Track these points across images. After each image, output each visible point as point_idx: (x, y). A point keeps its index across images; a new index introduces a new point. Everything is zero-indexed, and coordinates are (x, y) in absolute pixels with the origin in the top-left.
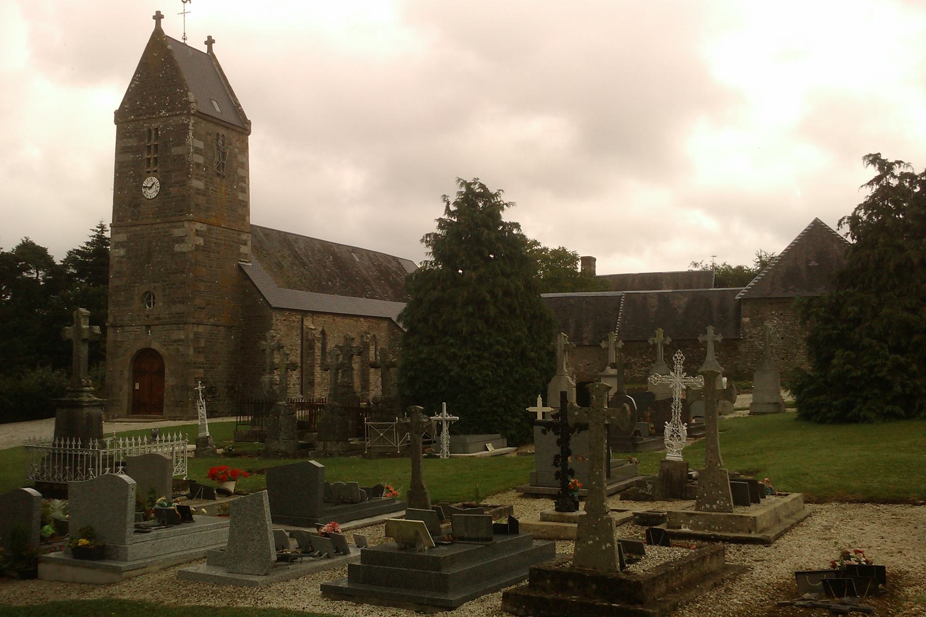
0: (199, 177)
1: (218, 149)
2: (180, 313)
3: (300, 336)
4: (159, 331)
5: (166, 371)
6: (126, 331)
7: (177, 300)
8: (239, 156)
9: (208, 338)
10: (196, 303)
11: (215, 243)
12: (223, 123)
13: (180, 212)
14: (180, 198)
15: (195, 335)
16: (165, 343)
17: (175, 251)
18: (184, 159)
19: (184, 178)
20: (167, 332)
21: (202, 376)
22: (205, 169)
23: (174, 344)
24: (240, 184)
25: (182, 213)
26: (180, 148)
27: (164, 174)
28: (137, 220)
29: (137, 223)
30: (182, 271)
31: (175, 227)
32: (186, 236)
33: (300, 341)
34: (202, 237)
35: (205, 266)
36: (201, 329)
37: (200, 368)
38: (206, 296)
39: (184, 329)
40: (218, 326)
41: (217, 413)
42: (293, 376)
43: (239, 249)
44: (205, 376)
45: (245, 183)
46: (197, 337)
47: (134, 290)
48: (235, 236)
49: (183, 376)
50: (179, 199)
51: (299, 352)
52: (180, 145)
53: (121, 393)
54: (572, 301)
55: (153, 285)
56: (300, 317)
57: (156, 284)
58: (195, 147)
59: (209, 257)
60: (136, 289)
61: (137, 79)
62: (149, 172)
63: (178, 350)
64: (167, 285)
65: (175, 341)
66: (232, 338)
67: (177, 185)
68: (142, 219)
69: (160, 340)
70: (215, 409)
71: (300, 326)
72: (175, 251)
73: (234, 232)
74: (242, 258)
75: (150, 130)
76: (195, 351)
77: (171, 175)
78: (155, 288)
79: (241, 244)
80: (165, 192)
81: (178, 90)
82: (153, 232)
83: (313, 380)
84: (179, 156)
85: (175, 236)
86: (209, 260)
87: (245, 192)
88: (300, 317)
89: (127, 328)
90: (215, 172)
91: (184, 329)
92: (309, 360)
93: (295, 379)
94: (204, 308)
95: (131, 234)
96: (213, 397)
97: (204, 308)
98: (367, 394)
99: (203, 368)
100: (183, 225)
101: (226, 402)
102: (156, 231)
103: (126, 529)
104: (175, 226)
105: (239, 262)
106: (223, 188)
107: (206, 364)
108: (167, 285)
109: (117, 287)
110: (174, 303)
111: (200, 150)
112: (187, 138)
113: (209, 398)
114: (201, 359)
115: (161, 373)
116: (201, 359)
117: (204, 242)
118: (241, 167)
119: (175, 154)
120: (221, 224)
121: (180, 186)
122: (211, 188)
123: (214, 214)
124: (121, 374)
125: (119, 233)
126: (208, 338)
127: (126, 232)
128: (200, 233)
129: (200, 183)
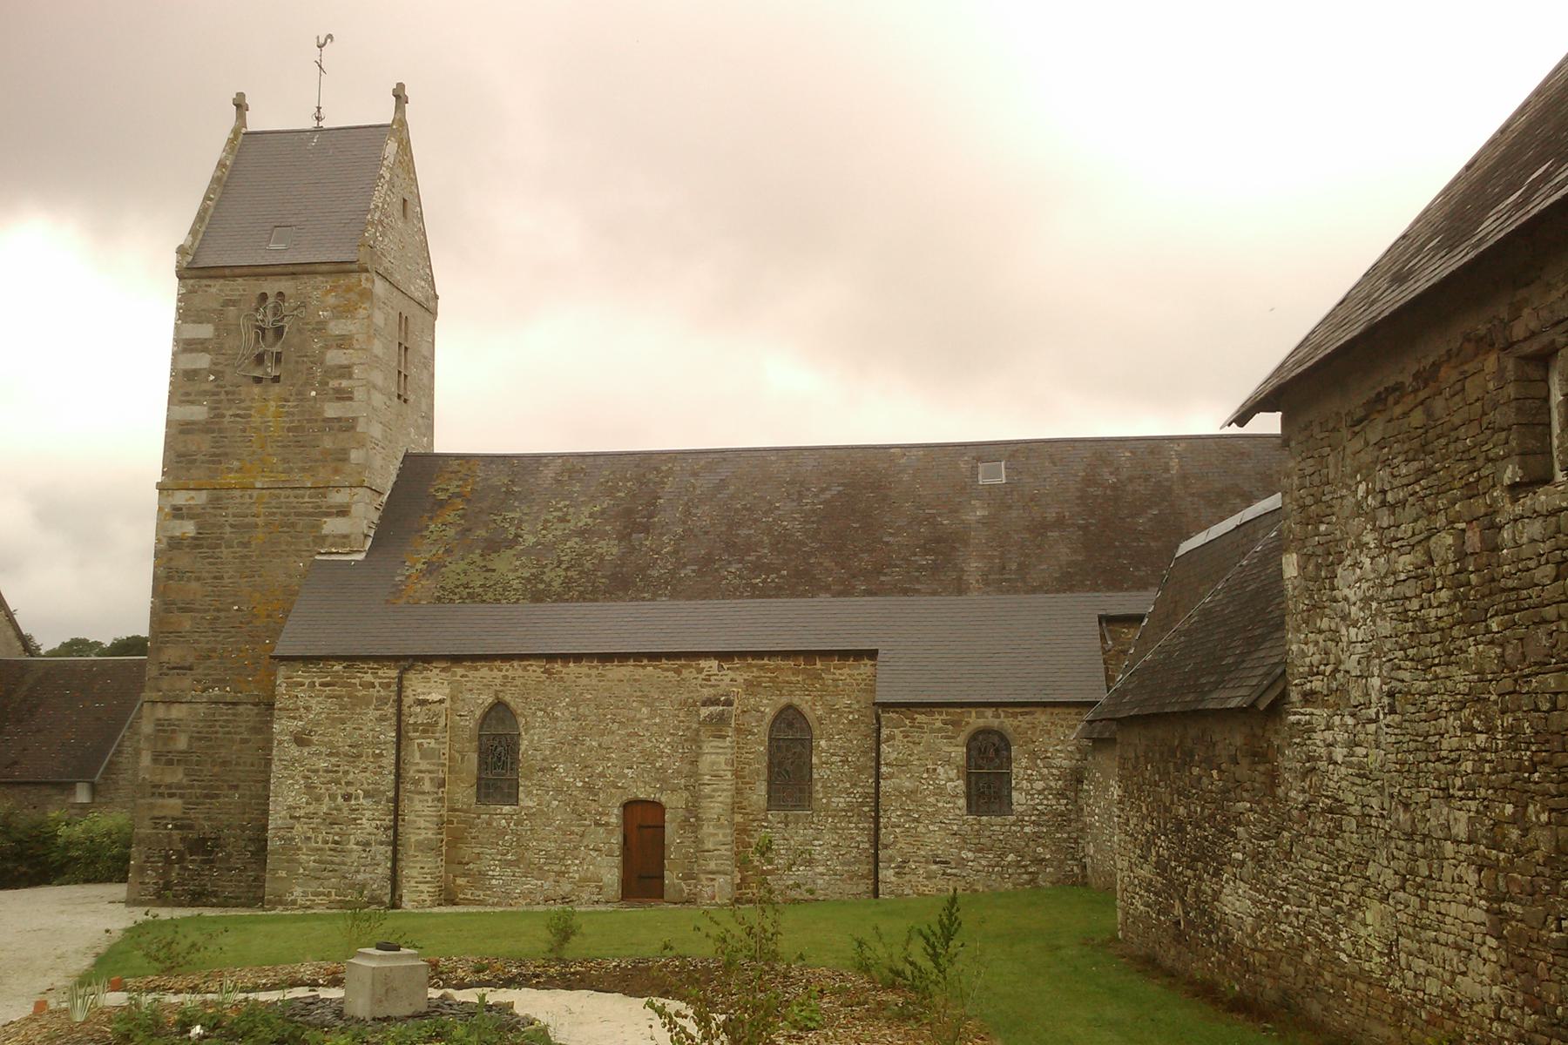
9: (199, 732)
10: (164, 658)
12: (271, 270)
15: (157, 725)
21: (178, 814)
34: (191, 518)
35: (198, 579)
36: (177, 712)
38: (196, 642)
40: (235, 704)
41: (216, 896)
42: (364, 821)
44: (184, 813)
56: (394, 673)
70: (209, 888)
71: (394, 696)
73: (302, 492)
74: (332, 545)
76: (155, 760)
88: (394, 673)
94: (190, 668)
96: (205, 862)
97: (190, 668)
99: (182, 796)
103: (1499, 917)
106: (272, 403)
107: (192, 787)
113: (192, 861)
114: (177, 776)
116: (177, 776)
120: (253, 483)
123: (236, 464)
126: (199, 732)
128: (184, 511)
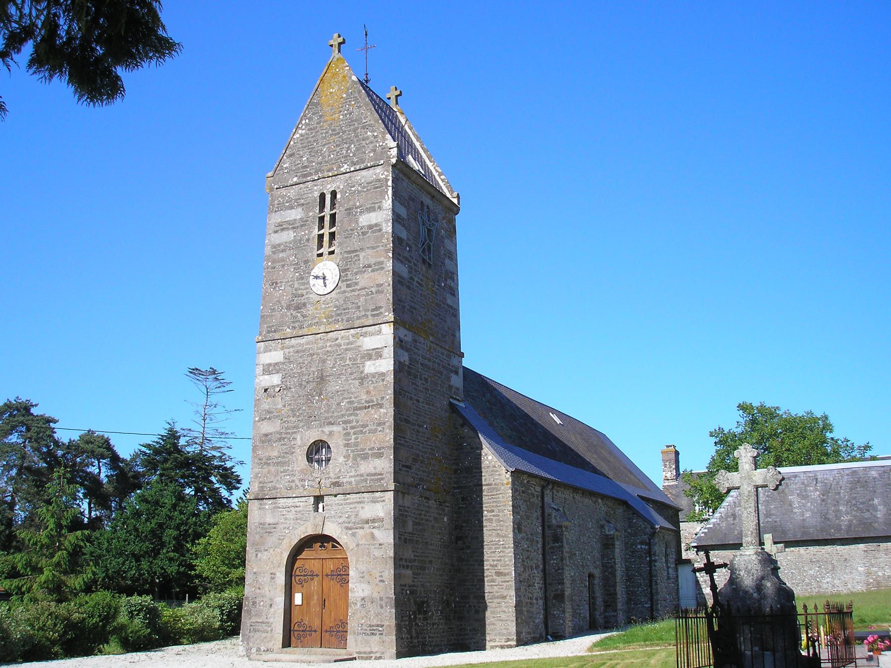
0: (401, 258)
1: (423, 224)
2: (375, 474)
3: (540, 520)
4: (339, 505)
5: (352, 573)
6: (280, 505)
7: (370, 452)
8: (446, 241)
11: (422, 364)
13: (373, 310)
14: (374, 290)
16: (349, 525)
17: (366, 372)
18: (380, 230)
19: (382, 259)
20: (352, 506)
22: (408, 249)
23: (366, 526)
24: (449, 281)
25: (378, 312)
26: (373, 215)
27: (346, 256)
28: (301, 328)
29: (300, 333)
30: (378, 404)
31: (364, 335)
32: (386, 347)
33: (540, 528)
35: (411, 399)
37: (407, 567)
39: (384, 501)
43: (449, 378)
45: (454, 281)
46: (402, 515)
47: (296, 439)
48: (445, 357)
49: (382, 581)
50: (372, 291)
51: (540, 545)
52: (374, 210)
53: (272, 610)
54: (873, 472)
55: (327, 429)
57: (335, 428)
58: (397, 213)
59: (415, 384)
60: (299, 437)
61: (304, 127)
62: (320, 255)
63: (373, 536)
64: (352, 428)
65: (367, 522)
66: (445, 520)
67: (370, 269)
68: (311, 325)
69: (340, 521)
72: (366, 372)
75: (322, 196)
77: (358, 256)
78: (331, 433)
79: (452, 371)
80: (348, 283)
81: (369, 133)
82: (328, 345)
83: (563, 591)
84: (370, 227)
85: (365, 348)
86: (416, 389)
87: (454, 295)
89: (281, 501)
90: (420, 255)
91: (384, 501)
92: (554, 559)
93: (538, 590)
95: (291, 350)
98: (614, 616)
100: (380, 331)
101: (441, 627)
102: (333, 343)
104: (366, 333)
105: (451, 400)
108: (352, 428)
109: (266, 435)
110: (365, 457)
111: (403, 220)
112: (384, 199)
115: (341, 576)
117: (410, 359)
118: (449, 257)
119: (365, 224)
121: (373, 271)
122: (416, 279)
124: (273, 578)
125: (270, 351)
127: (282, 348)
129: (403, 267)
